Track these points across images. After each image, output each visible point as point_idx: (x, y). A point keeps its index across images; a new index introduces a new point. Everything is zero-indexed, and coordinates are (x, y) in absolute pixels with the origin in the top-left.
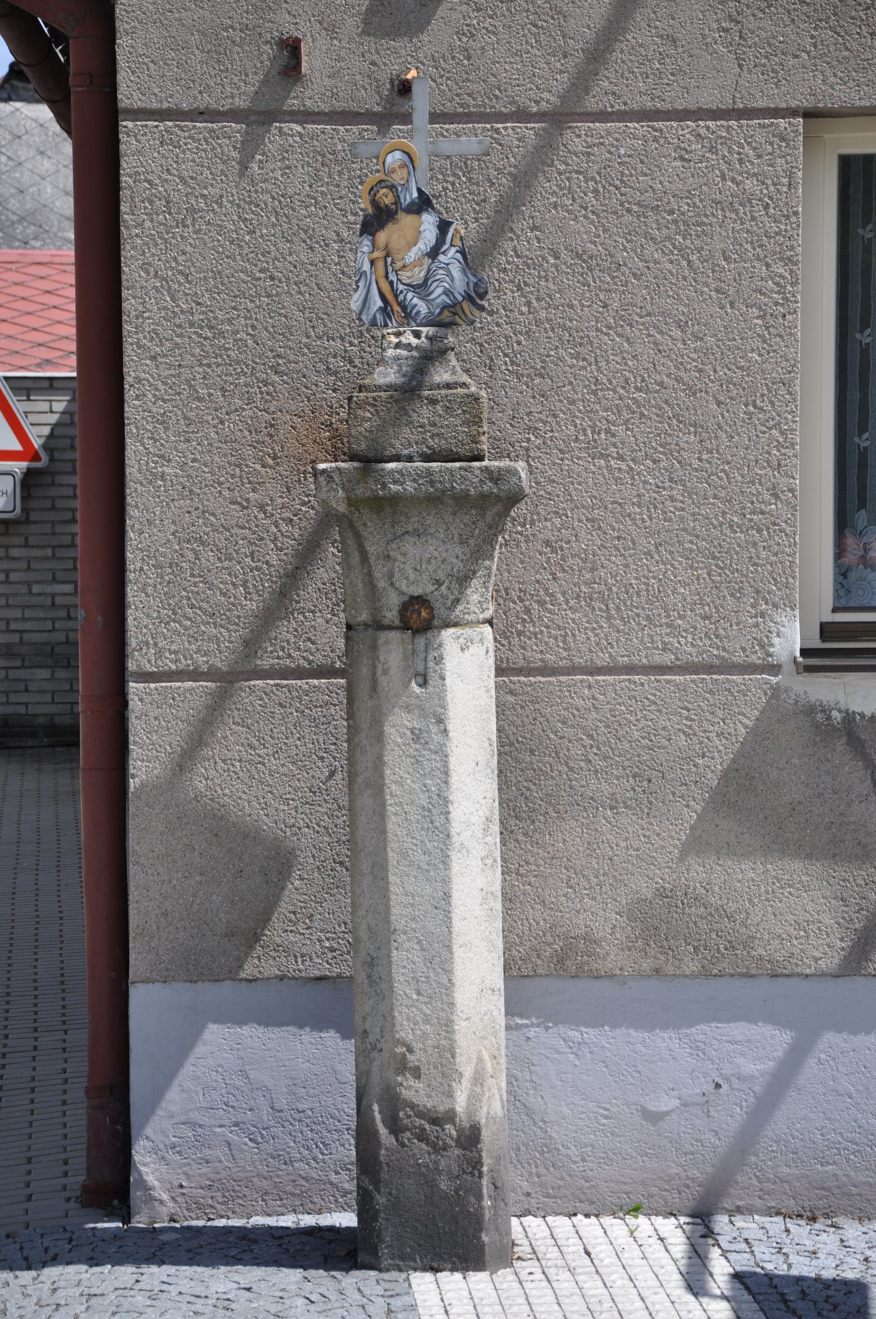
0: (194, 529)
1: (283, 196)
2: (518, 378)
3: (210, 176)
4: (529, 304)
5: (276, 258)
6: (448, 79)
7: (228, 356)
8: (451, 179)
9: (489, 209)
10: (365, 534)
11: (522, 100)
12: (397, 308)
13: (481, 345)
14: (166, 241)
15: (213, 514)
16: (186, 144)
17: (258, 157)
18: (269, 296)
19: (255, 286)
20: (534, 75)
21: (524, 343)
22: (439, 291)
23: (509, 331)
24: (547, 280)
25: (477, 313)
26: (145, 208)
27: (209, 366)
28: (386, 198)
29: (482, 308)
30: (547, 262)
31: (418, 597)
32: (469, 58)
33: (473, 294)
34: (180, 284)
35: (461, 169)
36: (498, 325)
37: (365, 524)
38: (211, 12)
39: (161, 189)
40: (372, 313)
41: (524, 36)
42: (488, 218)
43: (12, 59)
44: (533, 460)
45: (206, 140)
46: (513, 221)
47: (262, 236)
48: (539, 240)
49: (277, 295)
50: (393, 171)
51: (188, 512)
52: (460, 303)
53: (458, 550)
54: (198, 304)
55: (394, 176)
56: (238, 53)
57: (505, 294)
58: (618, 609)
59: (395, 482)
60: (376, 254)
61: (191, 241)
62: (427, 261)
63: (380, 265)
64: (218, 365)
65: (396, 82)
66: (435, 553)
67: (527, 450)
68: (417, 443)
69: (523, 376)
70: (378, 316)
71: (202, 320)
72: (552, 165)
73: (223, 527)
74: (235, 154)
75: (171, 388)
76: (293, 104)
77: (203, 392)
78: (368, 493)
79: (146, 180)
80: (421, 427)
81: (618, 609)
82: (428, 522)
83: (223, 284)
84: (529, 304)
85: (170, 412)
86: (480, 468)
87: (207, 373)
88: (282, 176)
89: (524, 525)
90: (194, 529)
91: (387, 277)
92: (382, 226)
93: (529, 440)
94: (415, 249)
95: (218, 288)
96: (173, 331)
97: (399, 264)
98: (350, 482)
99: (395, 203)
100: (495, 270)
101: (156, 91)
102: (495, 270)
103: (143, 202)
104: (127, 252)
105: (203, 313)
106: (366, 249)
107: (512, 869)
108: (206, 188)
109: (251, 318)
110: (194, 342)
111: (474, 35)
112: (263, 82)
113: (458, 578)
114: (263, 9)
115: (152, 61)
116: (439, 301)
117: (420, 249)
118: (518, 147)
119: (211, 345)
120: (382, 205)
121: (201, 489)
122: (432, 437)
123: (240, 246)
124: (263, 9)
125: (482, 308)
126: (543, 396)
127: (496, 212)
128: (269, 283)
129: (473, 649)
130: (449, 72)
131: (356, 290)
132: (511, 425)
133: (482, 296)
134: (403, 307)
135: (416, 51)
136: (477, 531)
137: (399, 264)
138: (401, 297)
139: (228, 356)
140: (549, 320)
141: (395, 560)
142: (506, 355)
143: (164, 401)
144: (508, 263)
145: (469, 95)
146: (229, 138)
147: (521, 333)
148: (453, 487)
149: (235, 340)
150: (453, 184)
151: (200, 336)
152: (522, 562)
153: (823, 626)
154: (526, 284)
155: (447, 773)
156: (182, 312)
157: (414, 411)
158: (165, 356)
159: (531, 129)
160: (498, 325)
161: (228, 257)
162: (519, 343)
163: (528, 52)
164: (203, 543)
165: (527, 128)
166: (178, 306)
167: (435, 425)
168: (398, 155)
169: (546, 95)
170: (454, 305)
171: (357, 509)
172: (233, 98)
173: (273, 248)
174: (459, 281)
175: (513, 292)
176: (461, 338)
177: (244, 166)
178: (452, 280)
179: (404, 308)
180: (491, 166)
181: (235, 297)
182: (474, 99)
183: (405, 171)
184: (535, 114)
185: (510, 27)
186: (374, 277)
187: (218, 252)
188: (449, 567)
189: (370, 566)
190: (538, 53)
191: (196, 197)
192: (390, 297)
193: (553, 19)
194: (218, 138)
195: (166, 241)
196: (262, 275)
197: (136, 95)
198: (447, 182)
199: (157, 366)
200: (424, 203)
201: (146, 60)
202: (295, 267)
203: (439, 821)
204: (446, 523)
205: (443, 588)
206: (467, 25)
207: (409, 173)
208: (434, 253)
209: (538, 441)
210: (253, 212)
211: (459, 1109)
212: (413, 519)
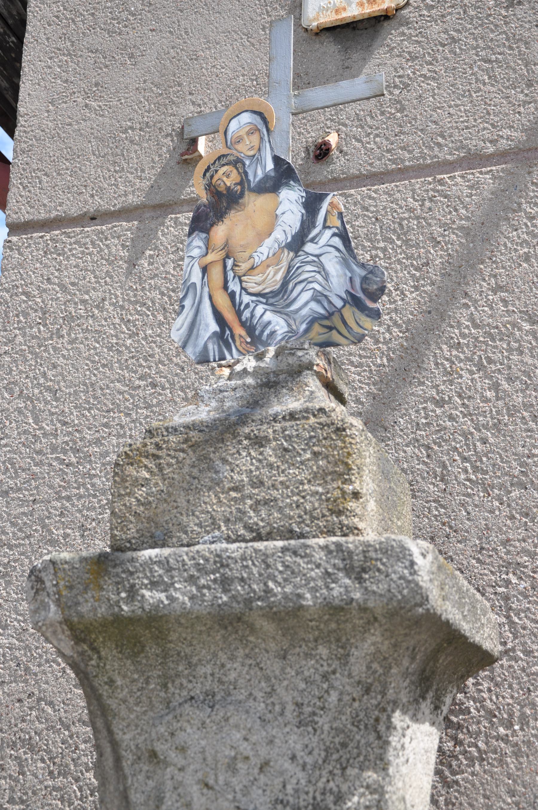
0: (23, 725)
1: (173, 291)
2: (485, 490)
3: (93, 280)
4: (496, 387)
5: (161, 362)
6: (377, 135)
7: (93, 485)
8: (382, 245)
9: (434, 274)
11: (473, 144)
12: (239, 331)
13: (428, 447)
14: (36, 355)
15: (51, 704)
16: (70, 250)
17: (148, 253)
18: (148, 406)
19: (132, 396)
20: (488, 113)
21: (491, 440)
22: (306, 296)
23: (468, 425)
24: (521, 353)
25: (367, 322)
26: (19, 322)
27: (68, 498)
29: (376, 315)
30: (520, 329)
32: (402, 110)
33: (360, 295)
34: (47, 402)
35: (394, 230)
36: (451, 418)
37: (111, 682)
38: (111, 118)
39: (39, 300)
40: (201, 342)
41: (472, 74)
42: (433, 284)
44: (517, 615)
45: (93, 243)
46: (467, 284)
47: (145, 338)
48: (505, 302)
49: (159, 404)
50: (239, 140)
51: (20, 701)
52: (339, 311)
53: (295, 741)
54: (65, 424)
55: (239, 147)
56: (136, 152)
57: (461, 377)
59: (154, 585)
60: (211, 257)
61: (65, 352)
62: (287, 256)
63: (216, 273)
64: (80, 497)
65: (312, 149)
66: (245, 748)
67: (507, 598)
68: (227, 521)
69: (492, 487)
70: (210, 346)
71: (67, 443)
72: (520, 209)
73: (62, 723)
74: (124, 253)
75: (20, 530)
76: (192, 192)
77: (58, 533)
78: (102, 611)
79: (24, 293)
80: (235, 489)
82: (233, 676)
83: (95, 398)
84: (496, 387)
85: (15, 561)
86: (325, 548)
87: (66, 509)
88: (174, 269)
89: (509, 725)
90: (23, 725)
91: (225, 287)
92: (220, 216)
93: (508, 583)
94: (269, 242)
95: (88, 402)
96: (33, 459)
97: (244, 266)
98: (70, 588)
99: (241, 183)
100: (444, 347)
101: (45, 202)
102: (444, 347)
103: (17, 316)
105: (69, 434)
106: (196, 252)
108: (87, 293)
109: (124, 436)
110: (55, 471)
111: (408, 85)
112: (160, 174)
114: (165, 105)
115: (46, 174)
116: (305, 311)
117: (276, 240)
118: (471, 195)
119: (74, 473)
120: (222, 189)
121: (39, 666)
122: (255, 508)
123: (119, 352)
124: (165, 105)
125: (376, 315)
126: (527, 515)
127: (443, 275)
128: (150, 390)
130: (377, 128)
131: (178, 314)
132: (479, 561)
133: (374, 297)
134: (250, 328)
135: (337, 114)
136: (333, 697)
137: (244, 266)
138: (246, 314)
139: (93, 485)
140: (527, 406)
141: (167, 764)
142: (465, 459)
143: (10, 547)
144: (463, 336)
145: (403, 148)
146: (119, 237)
147: (486, 427)
148: (268, 591)
149: (103, 464)
150: (384, 250)
151: (62, 462)
152: (512, 793)
154: (490, 361)
156: (45, 435)
157: (224, 461)
158: (19, 490)
159: (487, 173)
160: (451, 418)
161: (104, 366)
162: (484, 441)
163: (480, 90)
164: (32, 749)
165: (481, 173)
166: (41, 428)
167: (262, 483)
168: (246, 118)
169: (506, 132)
170: (331, 315)
171: (95, 650)
172: (126, 195)
173: (157, 350)
175: (471, 373)
176: (399, 440)
177: (132, 264)
178: (326, 277)
179: (250, 329)
180: (433, 222)
181: (108, 411)
182: (410, 152)
183: (255, 138)
184: (492, 155)
185: (454, 68)
186: (206, 289)
187: (93, 362)
190: (492, 89)
191: (76, 303)
192: (229, 316)
193: (511, 48)
194: (106, 239)
195: (36, 355)
196: (142, 383)
198: (377, 248)
199: (8, 502)
201: (39, 174)
202: (183, 369)
204: (268, 679)
206: (399, 77)
207: (262, 139)
208: (297, 243)
209: (523, 585)
210: (138, 312)
212: (201, 670)
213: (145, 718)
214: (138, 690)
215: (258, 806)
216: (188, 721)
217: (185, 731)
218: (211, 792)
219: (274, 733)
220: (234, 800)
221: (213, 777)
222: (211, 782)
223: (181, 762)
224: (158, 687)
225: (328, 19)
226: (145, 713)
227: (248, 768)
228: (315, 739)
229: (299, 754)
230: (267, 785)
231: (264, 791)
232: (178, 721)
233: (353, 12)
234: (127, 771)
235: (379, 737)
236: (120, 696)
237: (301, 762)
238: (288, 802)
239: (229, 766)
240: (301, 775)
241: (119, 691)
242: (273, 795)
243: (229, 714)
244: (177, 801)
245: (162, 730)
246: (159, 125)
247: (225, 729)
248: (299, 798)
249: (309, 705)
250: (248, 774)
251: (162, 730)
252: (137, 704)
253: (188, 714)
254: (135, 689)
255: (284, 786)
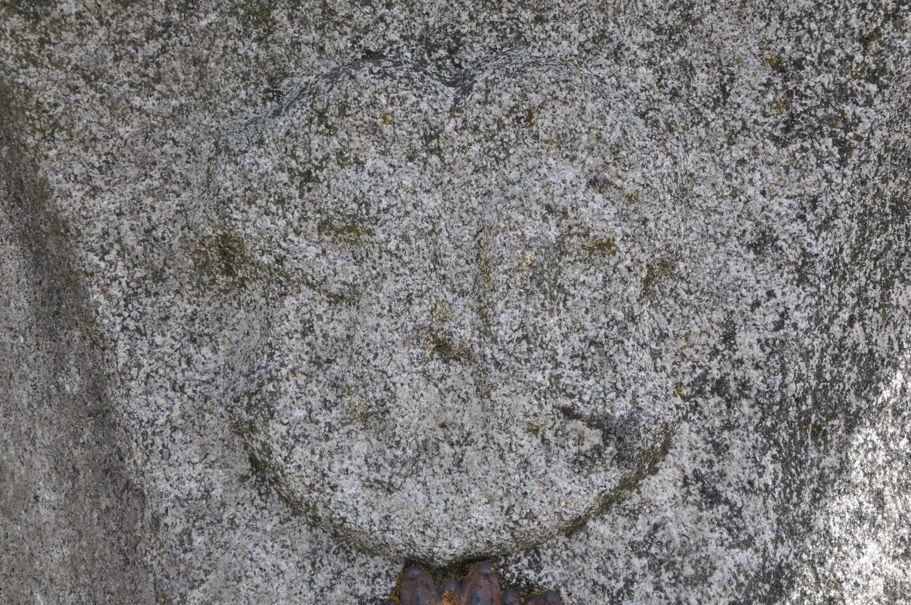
10: (44, 85)
31: (464, 567)
53: (771, 188)
66: (598, 213)
113: (772, 407)
141: (281, 279)
188: (704, 326)
189: (99, 343)
205: (662, 487)
213: (180, 135)
214: (151, 35)
215: (643, 402)
216: (374, 129)
217: (360, 164)
218: (456, 368)
219: (689, 162)
220: (556, 386)
221: (470, 317)
222: (464, 333)
223: (339, 268)
224: (233, 23)
226: (179, 115)
227: (607, 281)
228: (844, 179)
229: (787, 229)
230: (663, 336)
231: (656, 355)
232: (332, 130)
234: (108, 319)
236: (76, 55)
237: (792, 255)
238: (744, 385)
239: (537, 274)
240: (792, 297)
241: (69, 37)
242: (686, 366)
243: (535, 99)
244: (327, 405)
245: (266, 164)
247: (517, 153)
248: (784, 371)
249: (822, 63)
250: (606, 300)
251: (266, 164)
252: (146, 86)
253: (373, 104)
254: (135, 27)
255: (729, 337)
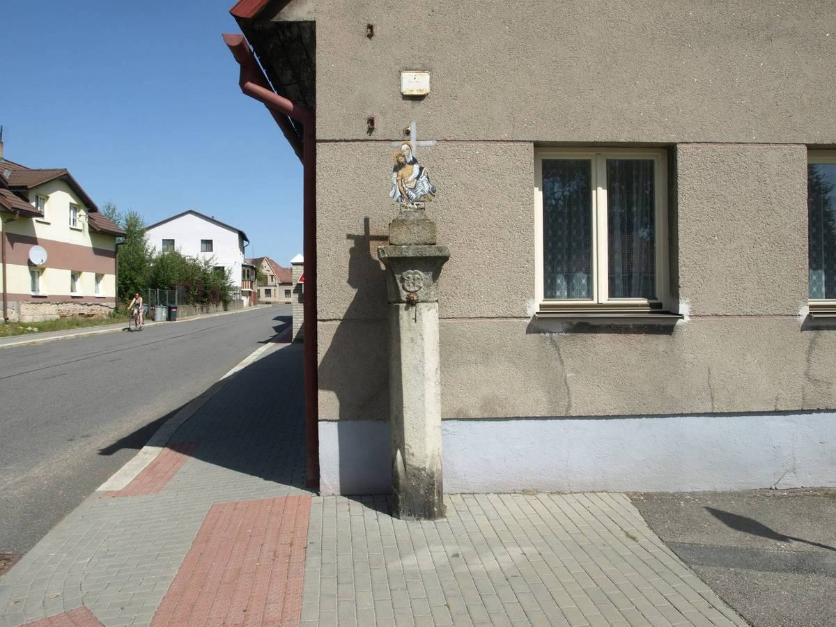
28: (402, 160)
43: (353, 245)
58: (477, 298)
62: (416, 180)
63: (400, 182)
81: (477, 298)
97: (406, 181)
104: (318, 184)
107: (444, 384)
125: (434, 196)
129: (432, 311)
137: (406, 181)
153: (540, 305)
155: (423, 353)
174: (427, 187)
179: (408, 196)
192: (403, 192)
197: (322, 135)
200: (414, 161)
203: (420, 369)
208: (418, 178)
211: (427, 467)
225: (408, 93)
233: (415, 93)
235: (419, 373)
246: (472, 197)
